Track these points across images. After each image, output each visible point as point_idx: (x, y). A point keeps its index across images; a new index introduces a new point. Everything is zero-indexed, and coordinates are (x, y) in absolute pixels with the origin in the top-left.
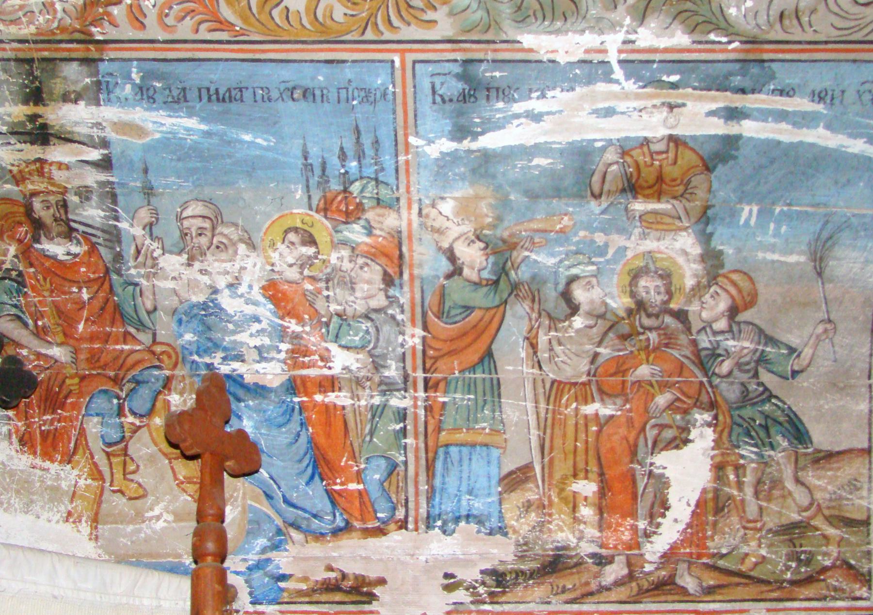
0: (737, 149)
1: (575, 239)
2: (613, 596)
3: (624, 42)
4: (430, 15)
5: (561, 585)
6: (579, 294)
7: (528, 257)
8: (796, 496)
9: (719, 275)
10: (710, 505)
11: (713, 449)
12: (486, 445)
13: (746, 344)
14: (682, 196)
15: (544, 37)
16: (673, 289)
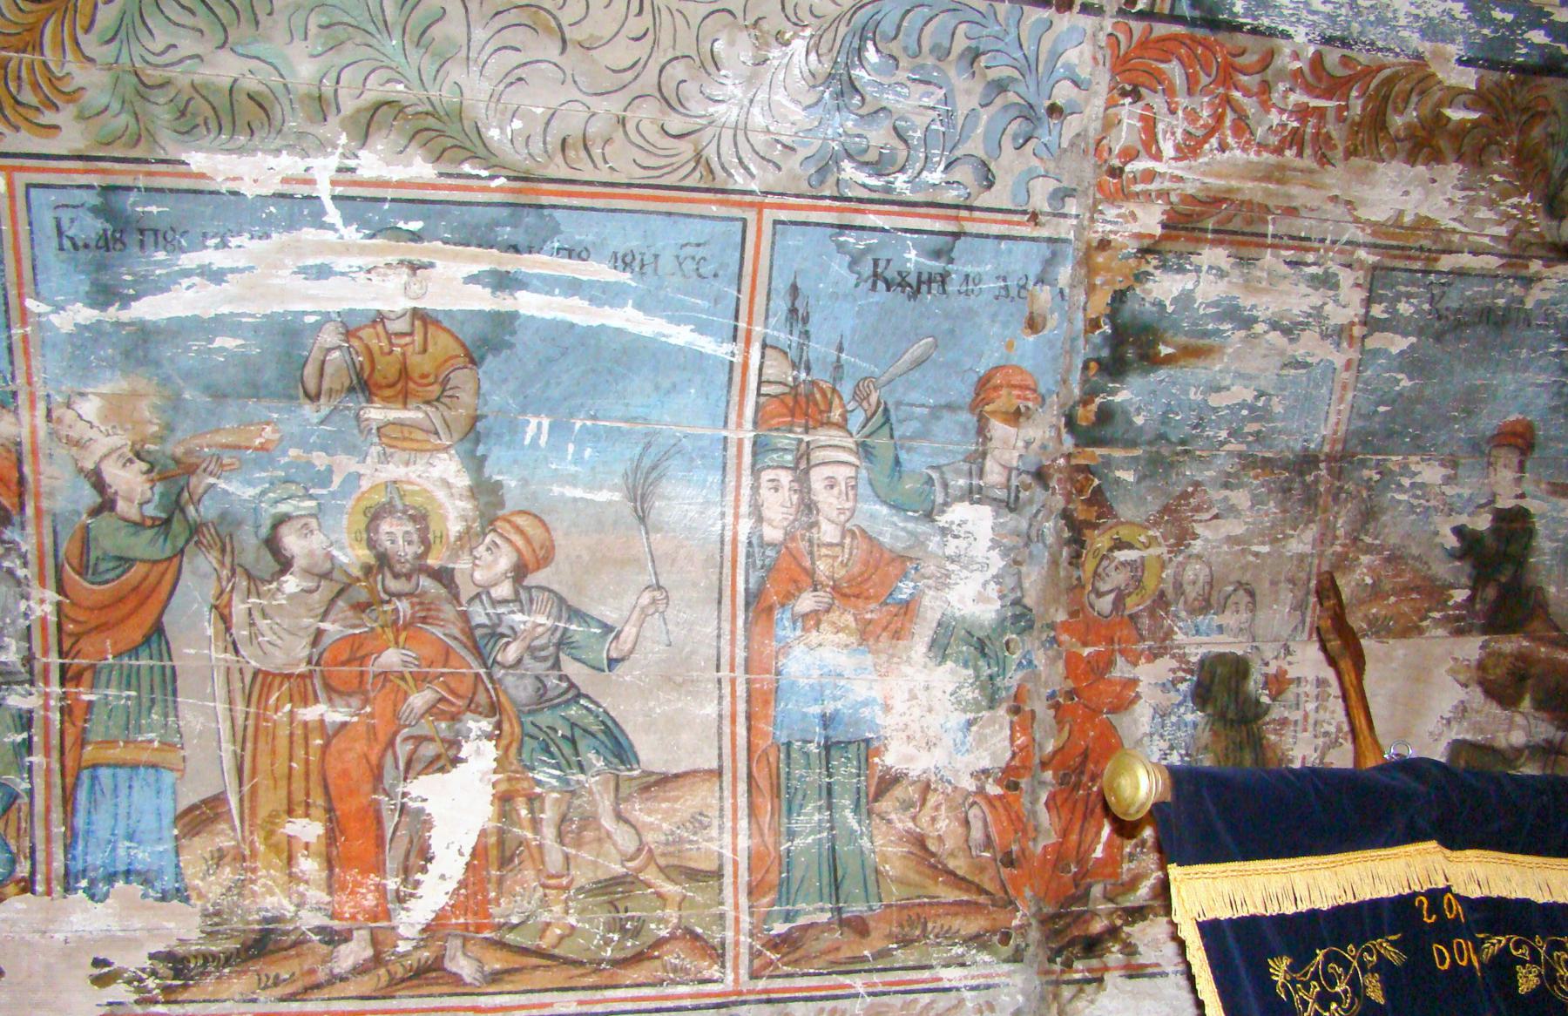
0: (513, 333)
1: (284, 460)
2: (352, 988)
3: (340, 170)
4: (48, 117)
5: (272, 975)
6: (291, 541)
7: (213, 485)
8: (618, 839)
9: (497, 519)
10: (493, 853)
11: (495, 772)
12: (154, 766)
13: (541, 619)
14: (438, 400)
15: (220, 157)
16: (431, 536)
